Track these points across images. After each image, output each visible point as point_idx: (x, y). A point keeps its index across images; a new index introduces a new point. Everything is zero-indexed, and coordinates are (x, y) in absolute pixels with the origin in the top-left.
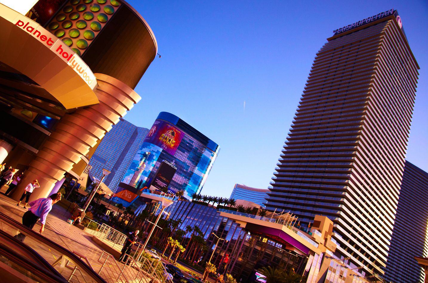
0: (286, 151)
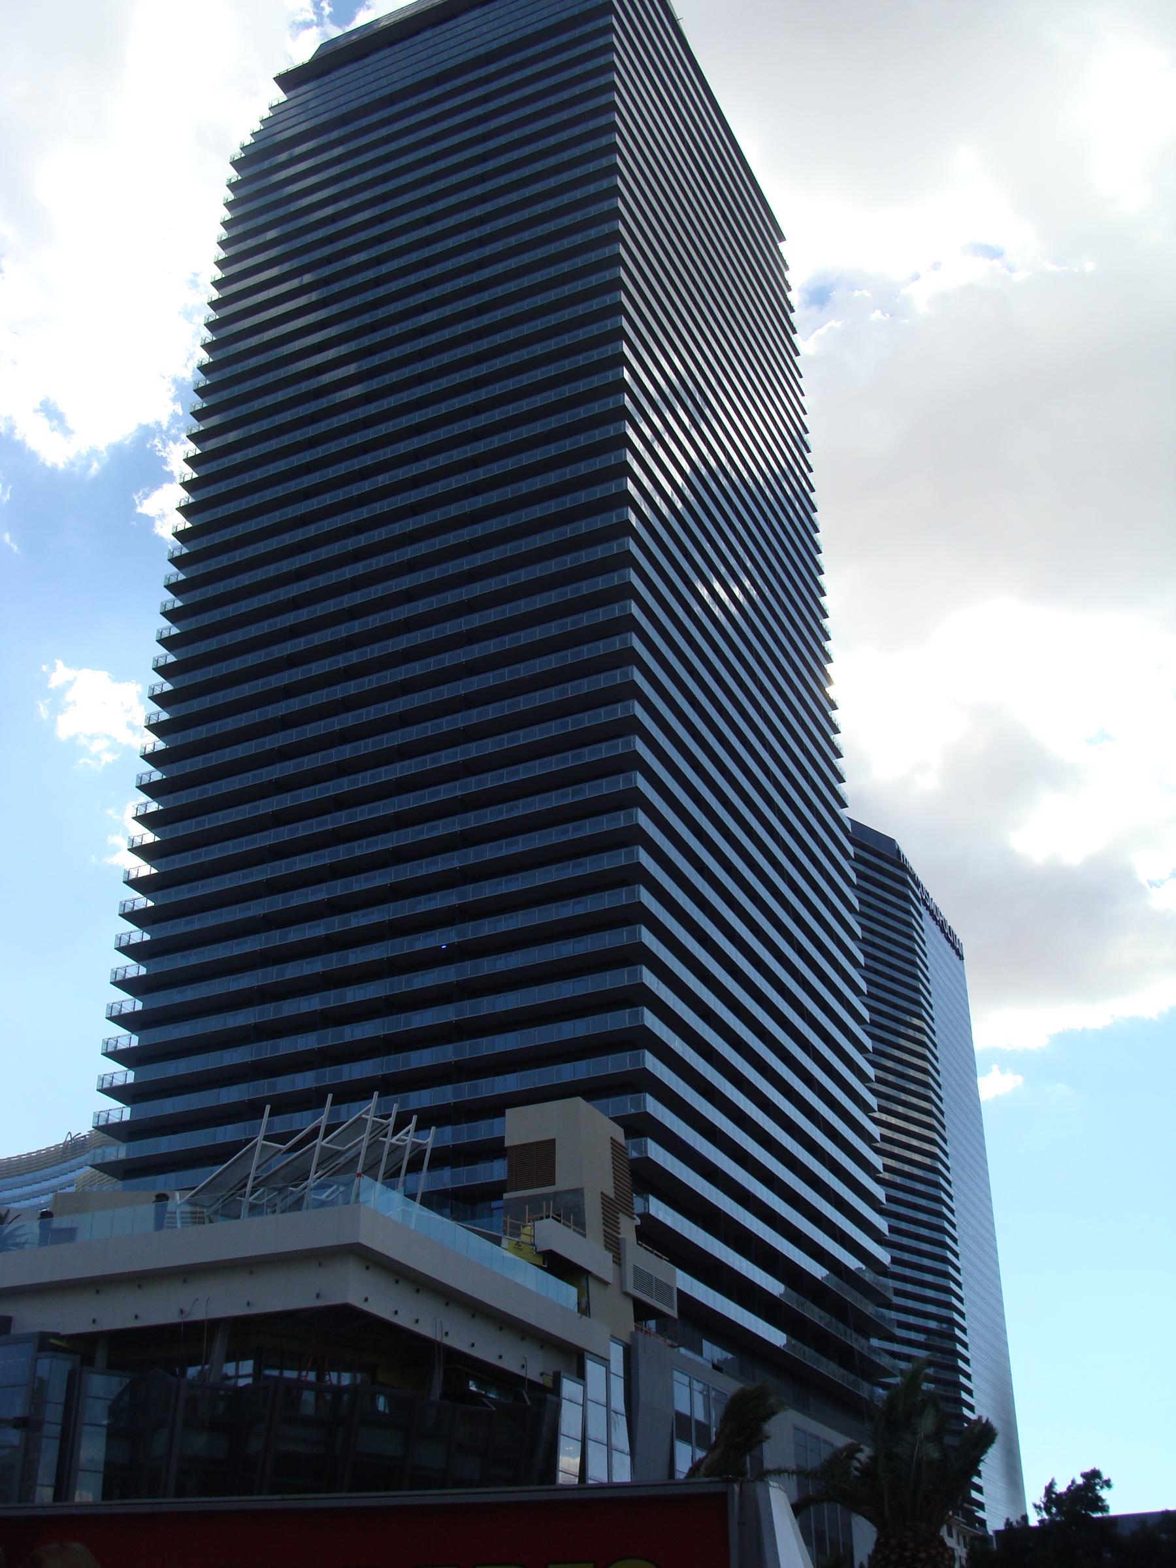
0: (143, 971)
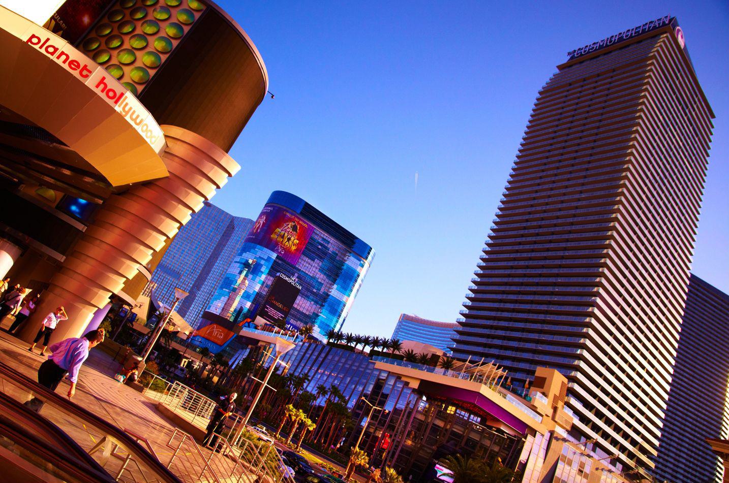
0: (487, 257)
